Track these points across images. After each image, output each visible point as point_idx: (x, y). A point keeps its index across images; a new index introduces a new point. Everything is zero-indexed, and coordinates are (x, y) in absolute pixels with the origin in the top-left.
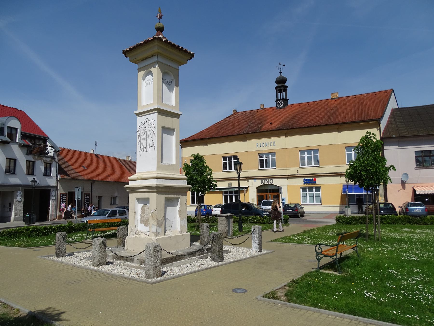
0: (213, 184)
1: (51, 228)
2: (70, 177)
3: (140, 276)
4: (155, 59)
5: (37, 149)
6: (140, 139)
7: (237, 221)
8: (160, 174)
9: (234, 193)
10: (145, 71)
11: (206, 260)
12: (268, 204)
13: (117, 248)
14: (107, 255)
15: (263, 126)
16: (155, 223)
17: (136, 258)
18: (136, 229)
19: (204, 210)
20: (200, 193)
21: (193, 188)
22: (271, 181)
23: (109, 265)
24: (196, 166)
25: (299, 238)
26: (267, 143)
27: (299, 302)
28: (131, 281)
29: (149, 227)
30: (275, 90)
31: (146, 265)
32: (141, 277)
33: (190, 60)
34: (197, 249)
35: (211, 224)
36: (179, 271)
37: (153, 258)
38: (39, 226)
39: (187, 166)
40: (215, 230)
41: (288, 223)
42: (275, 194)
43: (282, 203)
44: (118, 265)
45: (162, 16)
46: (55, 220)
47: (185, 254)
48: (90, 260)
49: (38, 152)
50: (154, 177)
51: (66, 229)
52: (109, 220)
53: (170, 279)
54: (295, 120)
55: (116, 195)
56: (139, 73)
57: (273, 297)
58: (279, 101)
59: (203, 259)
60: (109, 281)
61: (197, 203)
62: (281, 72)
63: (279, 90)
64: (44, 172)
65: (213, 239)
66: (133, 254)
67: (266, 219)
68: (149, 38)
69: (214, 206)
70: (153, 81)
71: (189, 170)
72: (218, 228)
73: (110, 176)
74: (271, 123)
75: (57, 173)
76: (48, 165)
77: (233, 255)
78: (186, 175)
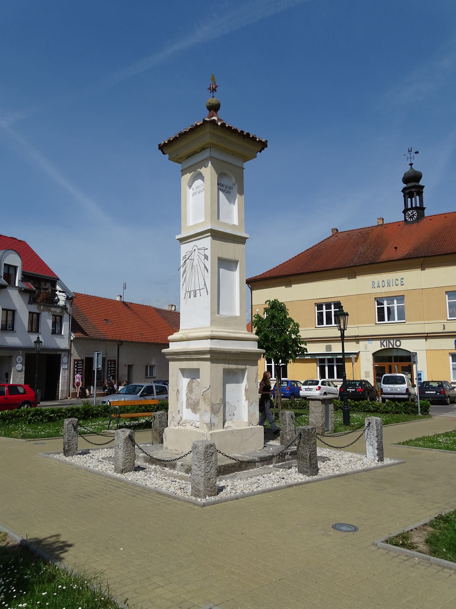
0: (300, 347)
1: (60, 411)
2: (87, 335)
3: (185, 491)
4: (206, 154)
5: (43, 295)
6: (185, 278)
7: (340, 408)
8: (216, 331)
9: (335, 361)
10: (191, 174)
11: (289, 470)
12: (393, 381)
13: (153, 444)
14: (137, 456)
15: (382, 253)
16: (208, 409)
17: (179, 463)
18: (179, 417)
19: (287, 388)
20: (280, 361)
21: (269, 354)
22: (398, 343)
23: (139, 471)
24: (273, 319)
25: (449, 440)
26: (390, 280)
27: (452, 556)
28: (171, 499)
29: (199, 414)
30: (402, 194)
31: (194, 475)
32: (185, 493)
33: (260, 152)
34: (275, 451)
35: (297, 411)
36: (244, 487)
37: (204, 464)
38: (43, 408)
39: (259, 320)
40: (305, 421)
41: (429, 414)
42: (406, 364)
43: (417, 379)
44: (152, 472)
45: (216, 87)
46: (68, 399)
47: (255, 459)
48: (112, 463)
49: (44, 300)
50: (207, 337)
51: (81, 413)
52: (141, 401)
53: (231, 500)
54: (438, 241)
55: (153, 363)
56: (183, 177)
57: (405, 545)
58: (409, 212)
59: (283, 469)
60: (138, 498)
61: (275, 377)
62: (412, 164)
63: (408, 194)
64: (52, 329)
65: (299, 438)
66: (174, 456)
67: (390, 406)
68: (197, 123)
69: (303, 383)
70: (204, 187)
71: (262, 326)
72: (309, 419)
73: (144, 334)
74: (396, 248)
75: (69, 330)
76: (58, 318)
77: (334, 465)
78: (256, 334)
